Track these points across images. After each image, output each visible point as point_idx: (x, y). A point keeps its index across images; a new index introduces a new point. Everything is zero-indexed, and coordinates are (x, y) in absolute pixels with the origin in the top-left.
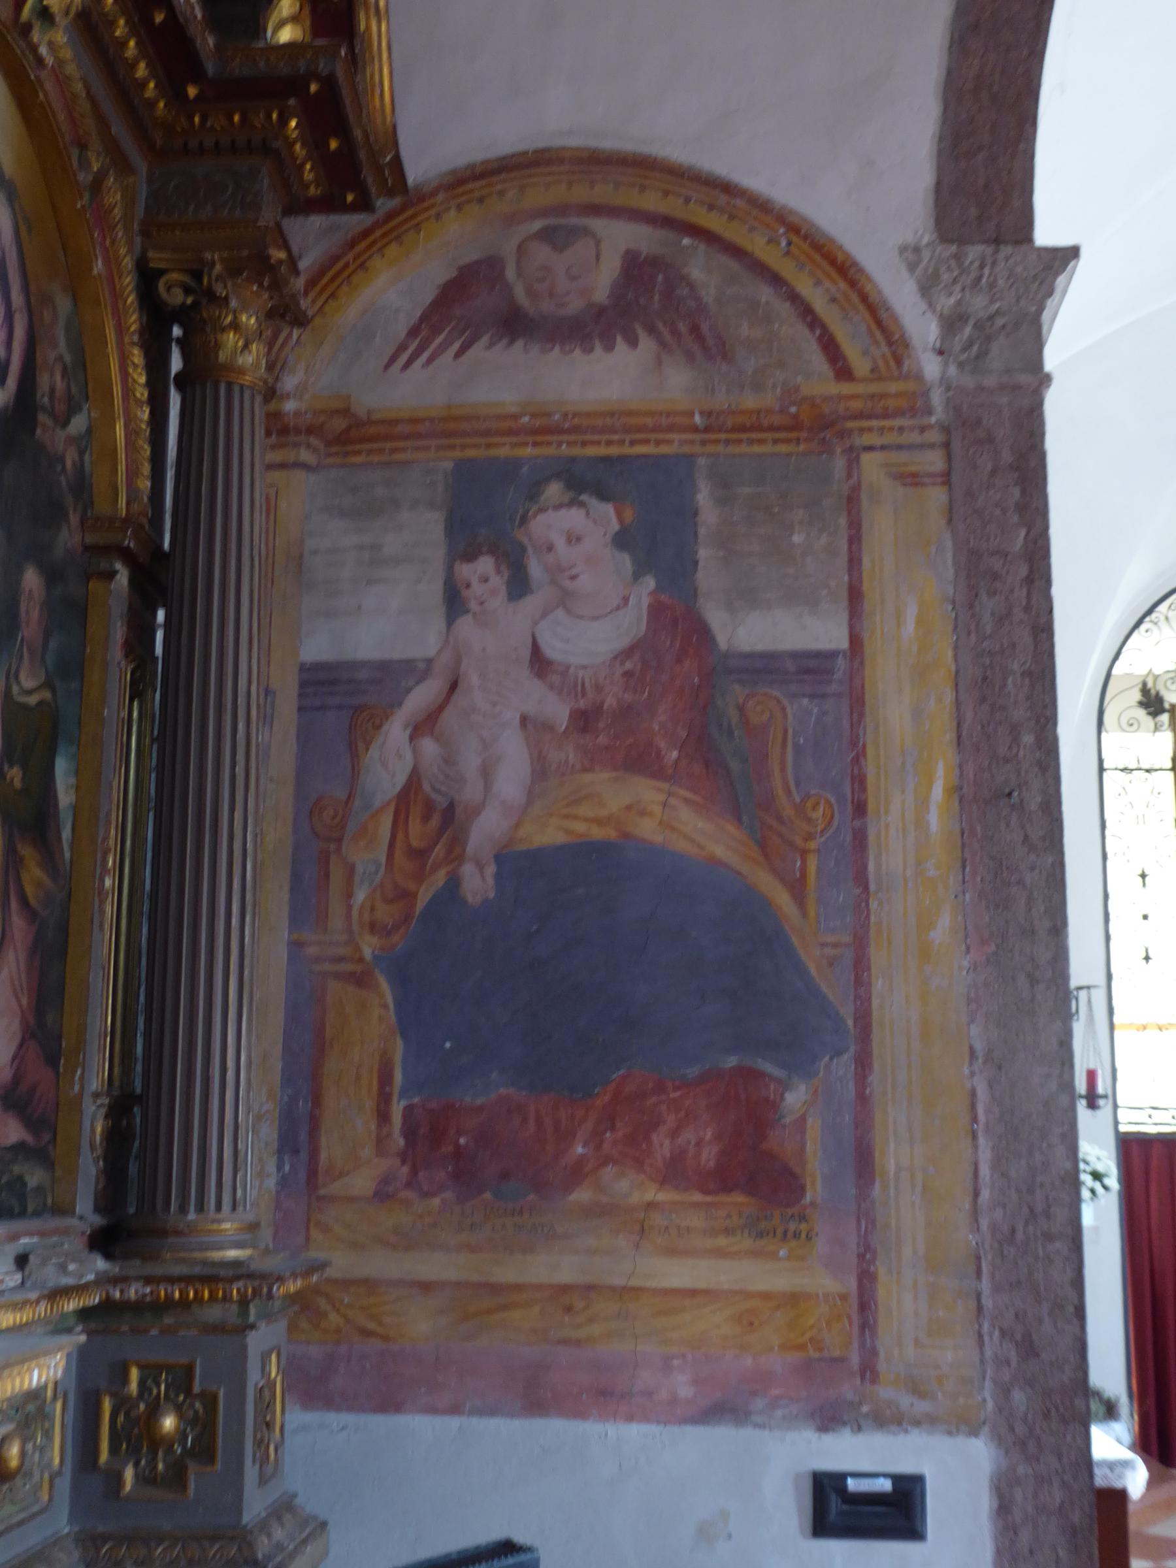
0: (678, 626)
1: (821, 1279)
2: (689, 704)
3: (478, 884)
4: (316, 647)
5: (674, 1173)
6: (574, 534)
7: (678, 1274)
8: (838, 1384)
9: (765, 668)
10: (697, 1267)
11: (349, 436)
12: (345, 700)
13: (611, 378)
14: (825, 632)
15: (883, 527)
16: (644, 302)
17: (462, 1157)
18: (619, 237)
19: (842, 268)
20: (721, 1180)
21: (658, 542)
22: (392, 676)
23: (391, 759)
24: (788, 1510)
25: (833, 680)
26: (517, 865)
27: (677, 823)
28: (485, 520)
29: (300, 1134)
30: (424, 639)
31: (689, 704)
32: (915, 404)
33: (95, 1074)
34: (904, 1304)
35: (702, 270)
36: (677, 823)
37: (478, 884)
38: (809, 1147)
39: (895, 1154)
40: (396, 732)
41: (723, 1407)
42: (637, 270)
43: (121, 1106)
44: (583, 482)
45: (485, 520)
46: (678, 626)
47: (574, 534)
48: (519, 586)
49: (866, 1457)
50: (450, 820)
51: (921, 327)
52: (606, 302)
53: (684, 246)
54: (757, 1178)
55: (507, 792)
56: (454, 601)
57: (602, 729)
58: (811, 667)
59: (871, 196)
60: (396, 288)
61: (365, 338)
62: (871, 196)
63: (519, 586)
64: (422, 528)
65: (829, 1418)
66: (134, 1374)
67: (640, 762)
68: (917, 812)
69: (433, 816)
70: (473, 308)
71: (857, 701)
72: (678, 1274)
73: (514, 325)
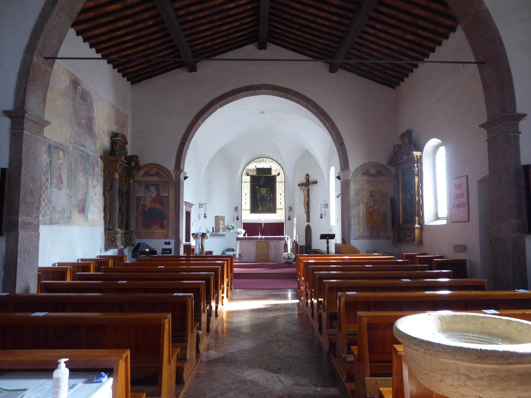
0: (158, 194)
1: (165, 231)
2: (159, 199)
3: (147, 210)
4: (137, 195)
5: (158, 226)
6: (152, 188)
7: (157, 231)
8: (166, 237)
9: (164, 197)
10: (159, 231)
11: (139, 182)
12: (139, 199)
13: (155, 179)
14: (167, 195)
15: (170, 188)
16: (157, 174)
17: (146, 225)
18: (156, 169)
19: (169, 172)
20: (160, 226)
21: (157, 189)
22: (142, 197)
23: (142, 202)
24: (163, 243)
25: (167, 198)
26: (149, 209)
27: (158, 206)
28: (147, 188)
29: (137, 224)
30: (144, 195)
31: (159, 199)
32: (173, 181)
33: (125, 221)
34: (170, 233)
35: (160, 172)
36: (158, 206)
37: (147, 210)
38: (157, 204)
39: (170, 225)
40: (142, 201)
41: (160, 238)
42: (157, 171)
43: (126, 223)
44: (153, 185)
45: (147, 188)
46: (158, 194)
47: (152, 188)
48: (149, 192)
49: (167, 241)
50: (145, 206)
51: (174, 176)
52: (244, 330)
53: (158, 170)
54: (162, 226)
55: (148, 204)
56: (145, 193)
57: (154, 201)
58: (166, 197)
59: (171, 167)
60: (142, 172)
61: (139, 176)
62: (171, 167)
63: (149, 192)
64: (143, 188)
65: (166, 239)
66: (158, 365)
67: (156, 203)
68: (172, 206)
69: (144, 206)
70: (147, 174)
71: (169, 199)
72: (157, 231)
73: (149, 175)
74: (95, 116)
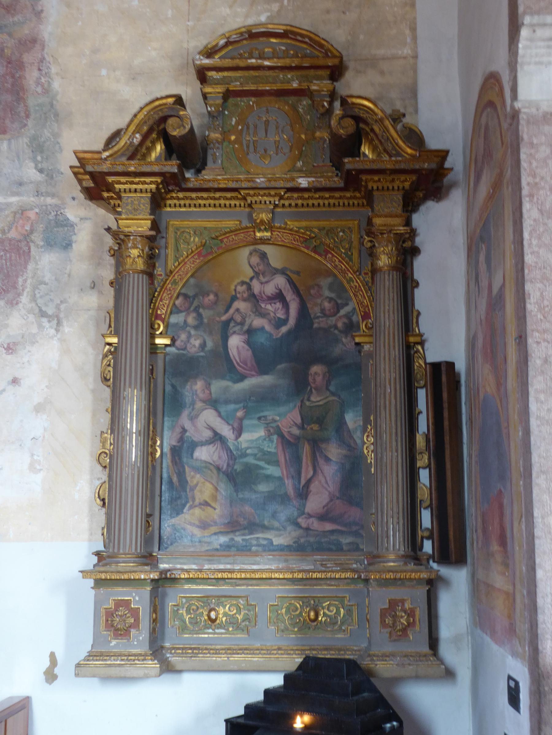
74: (47, 31)
